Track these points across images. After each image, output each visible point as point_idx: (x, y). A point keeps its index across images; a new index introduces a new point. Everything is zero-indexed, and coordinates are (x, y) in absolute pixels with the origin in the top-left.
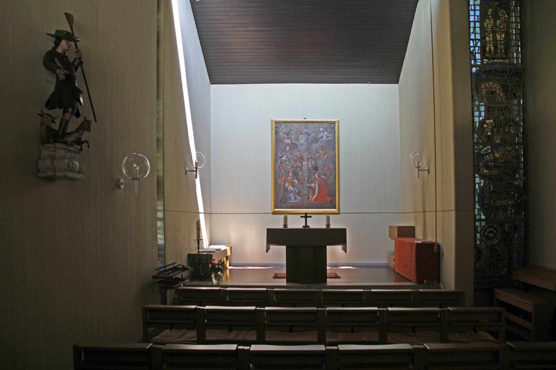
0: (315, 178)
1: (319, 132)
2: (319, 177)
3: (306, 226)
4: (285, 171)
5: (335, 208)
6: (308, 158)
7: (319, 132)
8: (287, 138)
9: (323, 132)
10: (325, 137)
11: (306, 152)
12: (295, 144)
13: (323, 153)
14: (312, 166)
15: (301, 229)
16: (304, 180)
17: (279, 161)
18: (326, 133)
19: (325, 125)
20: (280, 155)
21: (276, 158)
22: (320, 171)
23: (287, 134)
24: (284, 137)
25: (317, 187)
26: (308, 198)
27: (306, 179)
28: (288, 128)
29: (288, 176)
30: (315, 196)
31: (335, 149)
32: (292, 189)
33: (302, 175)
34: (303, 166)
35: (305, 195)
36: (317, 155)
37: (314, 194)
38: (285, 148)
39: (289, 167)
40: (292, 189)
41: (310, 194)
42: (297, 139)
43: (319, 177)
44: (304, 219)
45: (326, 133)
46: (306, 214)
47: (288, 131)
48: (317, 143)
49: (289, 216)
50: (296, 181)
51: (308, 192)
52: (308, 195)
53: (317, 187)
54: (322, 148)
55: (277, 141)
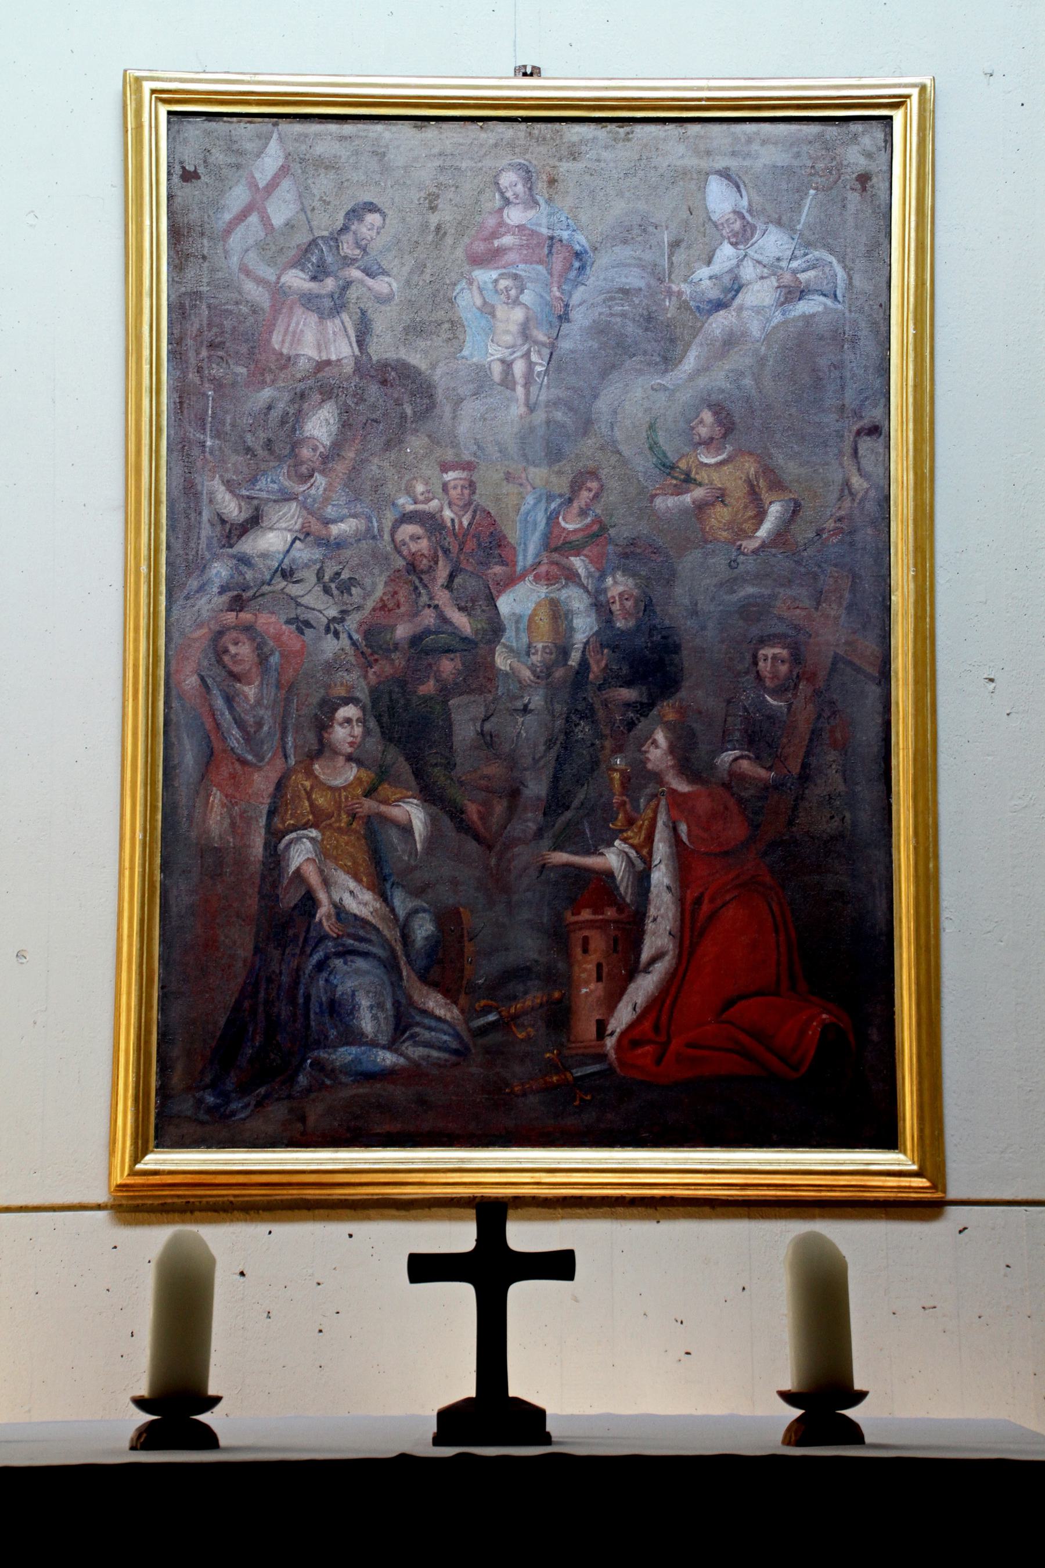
0: (639, 777)
1: (696, 234)
2: (686, 767)
3: (492, 1410)
4: (289, 690)
5: (889, 1141)
6: (558, 546)
7: (696, 234)
8: (309, 301)
9: (743, 236)
10: (759, 294)
11: (538, 474)
12: (405, 373)
13: (732, 480)
14: (608, 638)
15: (405, 1463)
16: (514, 794)
17: (220, 571)
18: (772, 243)
19: (770, 148)
20: (233, 509)
21: (190, 539)
22: (698, 693)
23: (317, 256)
24: (279, 293)
25: (661, 877)
26: (559, 1016)
27: (536, 788)
28: (323, 183)
29: (322, 749)
30: (644, 987)
31: (878, 431)
32: (360, 901)
33: (487, 740)
34: (495, 629)
35: (520, 973)
36: (666, 503)
37: (633, 970)
38: (292, 422)
39: (330, 647)
40: (360, 901)
41: (586, 967)
42: (433, 316)
43: (687, 757)
44: (461, 1298)
45: (772, 243)
46: (491, 1214)
47: (325, 223)
48: (668, 361)
49: (224, 1242)
50: (415, 814)
51: (559, 936)
52: (558, 978)
53: (661, 877)
54: (727, 425)
55: (207, 360)
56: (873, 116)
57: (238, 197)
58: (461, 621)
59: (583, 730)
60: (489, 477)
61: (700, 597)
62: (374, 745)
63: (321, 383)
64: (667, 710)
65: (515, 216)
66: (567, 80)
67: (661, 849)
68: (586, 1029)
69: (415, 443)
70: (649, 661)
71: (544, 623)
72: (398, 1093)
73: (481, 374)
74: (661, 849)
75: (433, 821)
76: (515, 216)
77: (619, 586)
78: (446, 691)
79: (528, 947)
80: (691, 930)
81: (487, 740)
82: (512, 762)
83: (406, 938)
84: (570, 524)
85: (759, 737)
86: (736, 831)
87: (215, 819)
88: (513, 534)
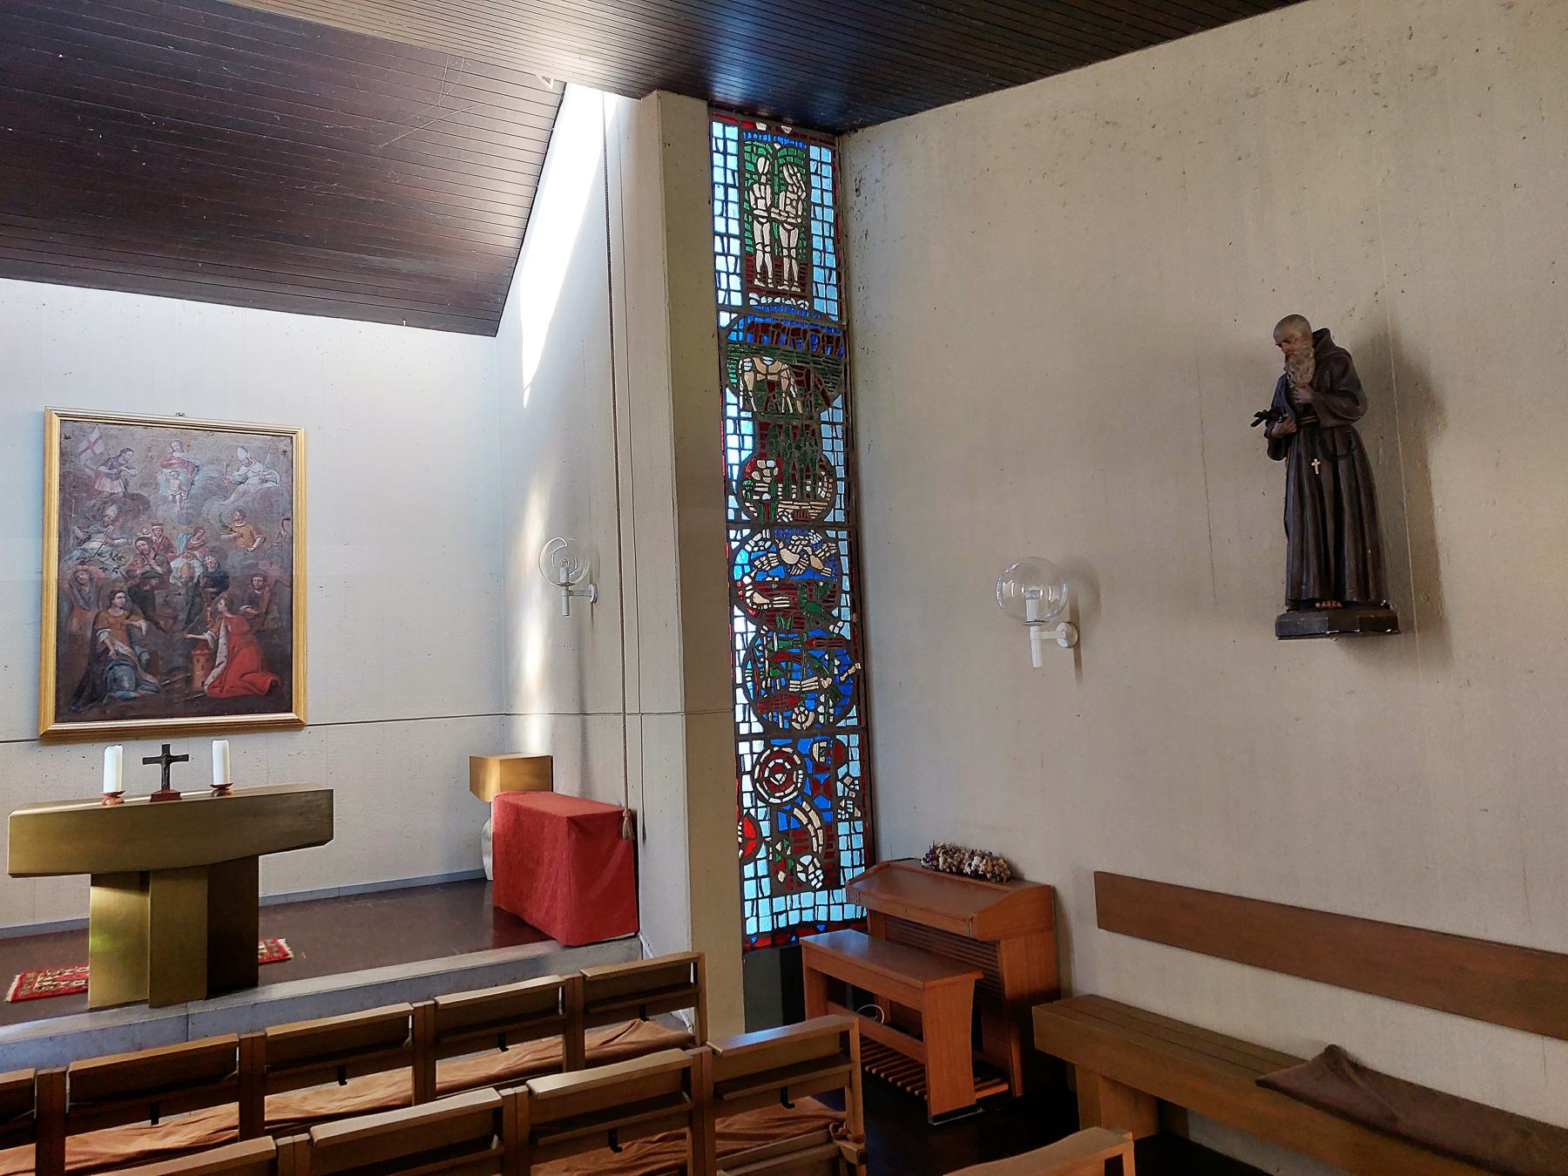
0: (215, 613)
1: (232, 462)
3: (166, 795)
7: (232, 462)
8: (107, 475)
9: (249, 464)
10: (254, 480)
14: (206, 574)
16: (175, 618)
17: (76, 553)
18: (257, 467)
19: (256, 441)
20: (81, 535)
24: (98, 474)
26: (189, 680)
27: (183, 616)
28: (113, 442)
32: (124, 649)
33: (167, 603)
34: (170, 571)
35: (178, 669)
40: (124, 649)
43: (231, 607)
48: (226, 498)
50: (143, 624)
52: (188, 669)
54: (244, 516)
55: (77, 495)
56: (289, 436)
57: (84, 445)
58: (159, 569)
59: (198, 600)
60: (168, 528)
61: (235, 562)
62: (130, 604)
63: (111, 499)
64: (225, 594)
65: (176, 454)
66: (191, 418)
67: (222, 633)
68: (197, 684)
69: (143, 518)
70: (219, 581)
71: (186, 569)
72: (136, 703)
73: (166, 498)
74: (222, 633)
75: (149, 627)
76: (176, 454)
77: (209, 560)
78: (153, 589)
79: (180, 661)
80: (231, 657)
81: (167, 603)
82: (175, 609)
83: (139, 658)
84: (194, 542)
85: (253, 602)
86: (246, 628)
87: (74, 625)
88: (175, 544)
